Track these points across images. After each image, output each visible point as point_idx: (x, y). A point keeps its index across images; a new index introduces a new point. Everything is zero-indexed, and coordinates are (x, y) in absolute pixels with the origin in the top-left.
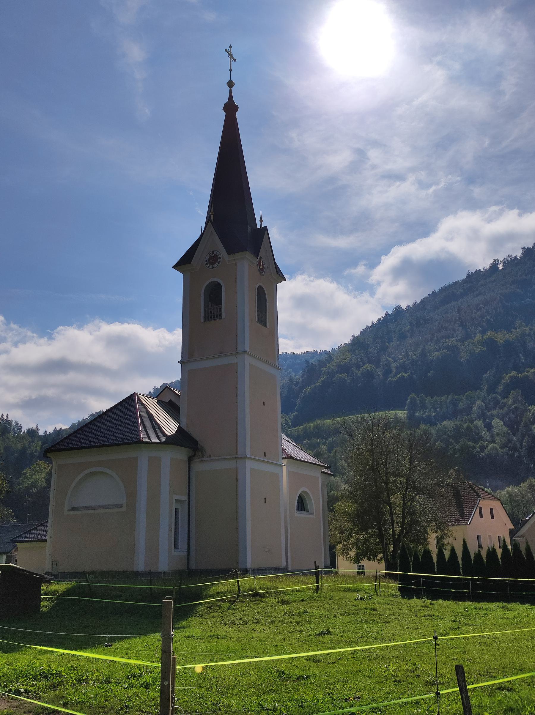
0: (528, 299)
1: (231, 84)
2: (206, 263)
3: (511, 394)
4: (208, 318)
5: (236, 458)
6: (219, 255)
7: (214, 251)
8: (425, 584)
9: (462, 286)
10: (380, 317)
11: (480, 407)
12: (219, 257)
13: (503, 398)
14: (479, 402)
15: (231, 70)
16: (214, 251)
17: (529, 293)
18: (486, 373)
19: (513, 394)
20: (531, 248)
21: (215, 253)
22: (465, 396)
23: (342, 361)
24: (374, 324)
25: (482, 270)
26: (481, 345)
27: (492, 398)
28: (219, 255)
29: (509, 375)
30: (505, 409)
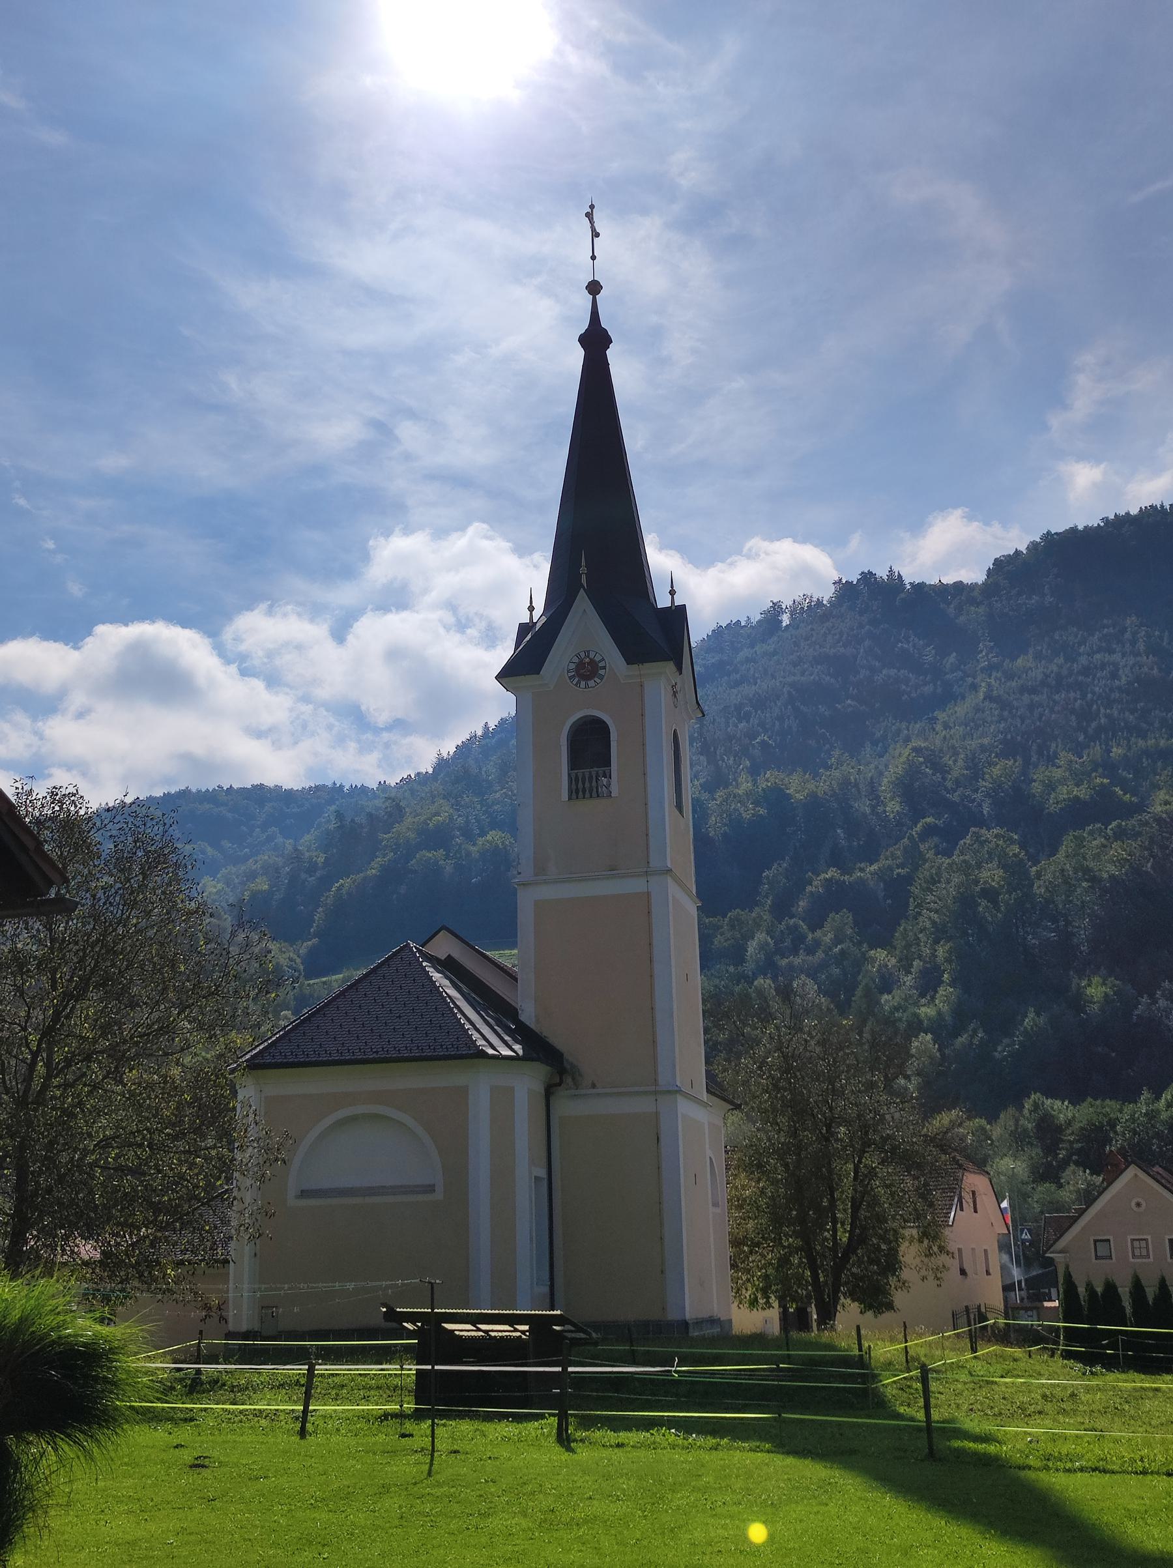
0: (849, 701)
1: (594, 288)
2: (570, 674)
3: (829, 920)
4: (577, 792)
5: (656, 1092)
6: (600, 661)
7: (588, 651)
8: (1127, 1346)
9: (702, 659)
10: (505, 715)
11: (763, 947)
12: (600, 665)
13: (813, 929)
14: (761, 936)
15: (593, 258)
16: (588, 651)
17: (851, 688)
18: (769, 869)
19: (833, 919)
20: (855, 583)
21: (592, 656)
22: (727, 920)
23: (431, 820)
24: (491, 729)
25: (743, 624)
26: (756, 803)
27: (788, 927)
28: (600, 661)
29: (823, 876)
30: (820, 954)
